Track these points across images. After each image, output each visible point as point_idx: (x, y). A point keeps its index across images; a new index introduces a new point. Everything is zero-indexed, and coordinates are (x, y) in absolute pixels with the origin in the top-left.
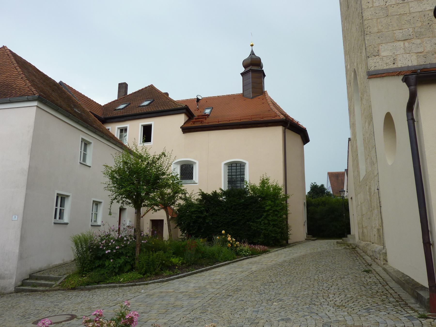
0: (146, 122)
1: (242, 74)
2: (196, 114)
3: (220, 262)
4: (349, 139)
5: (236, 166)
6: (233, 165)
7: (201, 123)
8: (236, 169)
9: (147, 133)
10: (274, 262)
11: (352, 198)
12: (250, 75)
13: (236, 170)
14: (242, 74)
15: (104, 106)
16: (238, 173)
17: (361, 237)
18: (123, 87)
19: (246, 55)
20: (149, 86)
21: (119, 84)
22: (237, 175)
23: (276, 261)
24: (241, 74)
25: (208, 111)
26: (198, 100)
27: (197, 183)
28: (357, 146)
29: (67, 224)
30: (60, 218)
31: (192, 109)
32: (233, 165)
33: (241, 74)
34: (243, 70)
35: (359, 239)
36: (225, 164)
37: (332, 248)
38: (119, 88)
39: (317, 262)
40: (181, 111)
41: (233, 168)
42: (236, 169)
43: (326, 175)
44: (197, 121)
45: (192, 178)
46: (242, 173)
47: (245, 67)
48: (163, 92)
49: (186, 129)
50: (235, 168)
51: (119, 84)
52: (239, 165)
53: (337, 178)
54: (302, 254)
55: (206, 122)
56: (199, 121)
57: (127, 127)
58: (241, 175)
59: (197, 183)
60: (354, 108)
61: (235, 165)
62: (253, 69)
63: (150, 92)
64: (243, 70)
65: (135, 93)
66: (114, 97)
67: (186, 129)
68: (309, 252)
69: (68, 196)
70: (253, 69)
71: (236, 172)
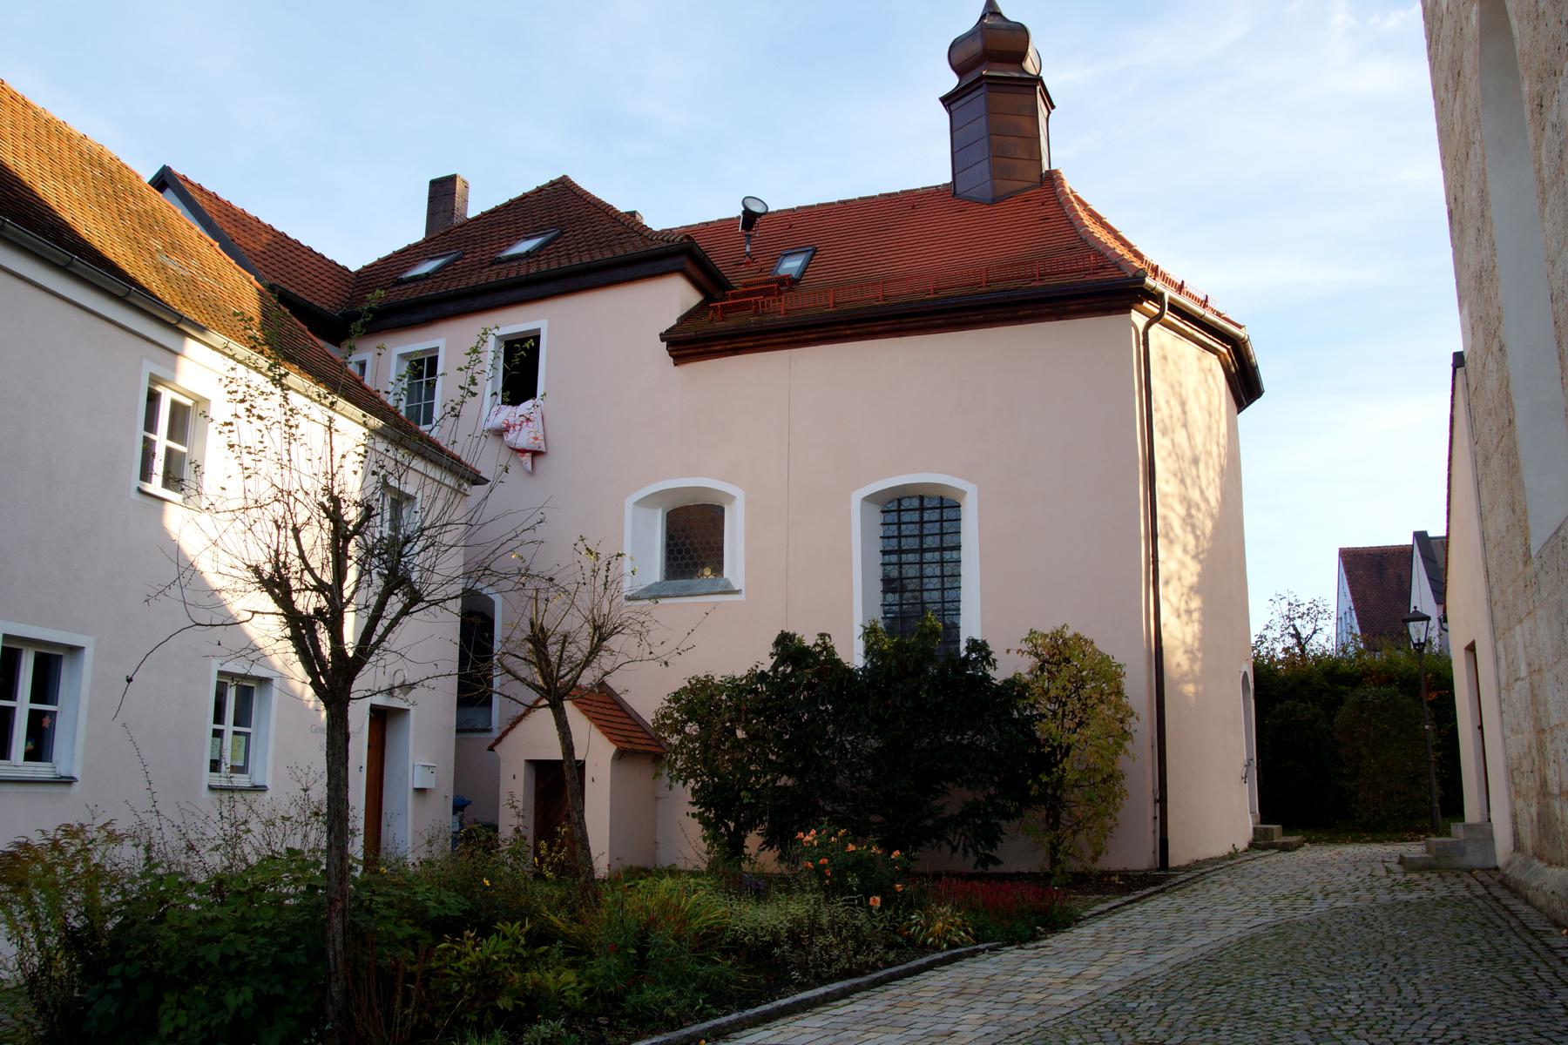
0: (515, 321)
1: (947, 100)
2: (739, 278)
3: (802, 987)
4: (1459, 360)
5: (922, 509)
6: (906, 504)
7: (756, 313)
8: (922, 522)
9: (520, 372)
10: (1083, 988)
11: (1471, 648)
12: (978, 99)
13: (917, 531)
14: (947, 100)
15: (359, 272)
16: (930, 542)
17: (1528, 841)
18: (443, 192)
19: (968, 18)
20: (552, 184)
21: (433, 183)
22: (922, 551)
23: (1094, 980)
24: (944, 100)
25: (791, 266)
26: (750, 218)
27: (737, 592)
28: (1505, 384)
29: (68, 781)
30: (30, 756)
31: (720, 260)
32: (906, 504)
33: (944, 100)
34: (951, 81)
35: (1518, 846)
36: (870, 499)
37: (1384, 897)
38: (432, 199)
39: (1316, 991)
40: (667, 263)
41: (906, 517)
42: (922, 522)
43: (1331, 570)
44: (736, 308)
45: (718, 568)
46: (948, 541)
47: (959, 69)
48: (623, 210)
49: (687, 343)
50: (915, 516)
51: (433, 183)
52: (936, 503)
53: (1375, 576)
54: (1233, 931)
55: (779, 309)
56: (746, 306)
57: (437, 349)
58: (942, 549)
59: (737, 592)
60: (1483, 192)
61: (916, 503)
62: (995, 78)
63: (559, 205)
64: (951, 81)
65: (492, 212)
66: (414, 230)
67: (687, 343)
68: (1269, 918)
69: (75, 650)
70: (995, 78)
71: (922, 536)
